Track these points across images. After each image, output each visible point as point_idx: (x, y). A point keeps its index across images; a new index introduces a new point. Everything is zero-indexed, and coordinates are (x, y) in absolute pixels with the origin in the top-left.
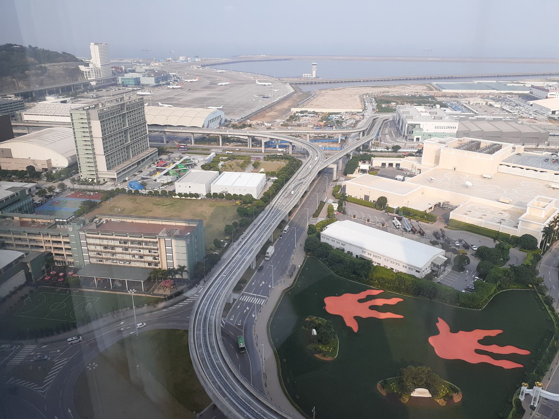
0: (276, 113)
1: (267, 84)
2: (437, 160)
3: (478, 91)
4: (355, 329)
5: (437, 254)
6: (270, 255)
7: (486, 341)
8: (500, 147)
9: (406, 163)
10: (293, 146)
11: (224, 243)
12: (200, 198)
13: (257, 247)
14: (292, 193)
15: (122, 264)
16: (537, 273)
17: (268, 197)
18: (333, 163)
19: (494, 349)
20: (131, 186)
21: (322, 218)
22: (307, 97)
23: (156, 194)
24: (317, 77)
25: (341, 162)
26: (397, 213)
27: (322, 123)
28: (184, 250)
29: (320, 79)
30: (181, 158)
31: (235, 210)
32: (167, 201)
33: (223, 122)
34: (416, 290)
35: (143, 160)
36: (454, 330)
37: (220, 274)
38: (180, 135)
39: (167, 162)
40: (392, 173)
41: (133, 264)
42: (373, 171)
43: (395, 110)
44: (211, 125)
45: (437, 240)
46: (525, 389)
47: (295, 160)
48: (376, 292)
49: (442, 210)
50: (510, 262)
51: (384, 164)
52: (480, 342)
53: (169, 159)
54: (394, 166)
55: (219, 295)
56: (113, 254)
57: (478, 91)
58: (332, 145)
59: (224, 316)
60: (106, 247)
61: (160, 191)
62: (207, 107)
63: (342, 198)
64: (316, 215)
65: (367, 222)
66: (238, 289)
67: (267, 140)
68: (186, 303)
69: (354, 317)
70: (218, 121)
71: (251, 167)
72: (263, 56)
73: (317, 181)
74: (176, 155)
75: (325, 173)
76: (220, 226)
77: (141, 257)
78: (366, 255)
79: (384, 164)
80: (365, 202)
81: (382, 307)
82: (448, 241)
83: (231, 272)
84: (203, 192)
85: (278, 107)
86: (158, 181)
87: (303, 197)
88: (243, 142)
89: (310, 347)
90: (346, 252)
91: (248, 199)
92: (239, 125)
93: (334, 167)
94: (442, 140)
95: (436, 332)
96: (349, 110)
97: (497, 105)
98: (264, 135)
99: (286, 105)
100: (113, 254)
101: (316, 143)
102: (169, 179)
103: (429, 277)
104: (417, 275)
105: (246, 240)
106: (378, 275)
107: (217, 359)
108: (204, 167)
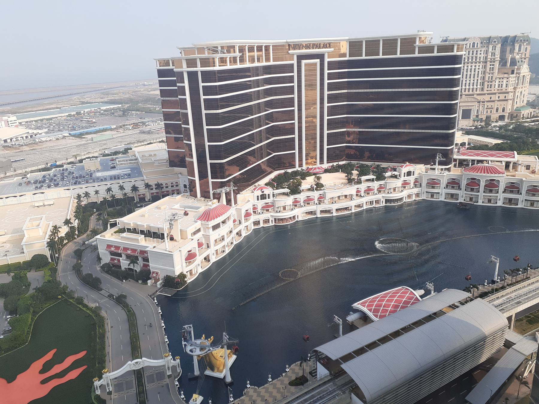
16: (60, 283)
19: (57, 369)
46: (97, 383)
50: (33, 286)
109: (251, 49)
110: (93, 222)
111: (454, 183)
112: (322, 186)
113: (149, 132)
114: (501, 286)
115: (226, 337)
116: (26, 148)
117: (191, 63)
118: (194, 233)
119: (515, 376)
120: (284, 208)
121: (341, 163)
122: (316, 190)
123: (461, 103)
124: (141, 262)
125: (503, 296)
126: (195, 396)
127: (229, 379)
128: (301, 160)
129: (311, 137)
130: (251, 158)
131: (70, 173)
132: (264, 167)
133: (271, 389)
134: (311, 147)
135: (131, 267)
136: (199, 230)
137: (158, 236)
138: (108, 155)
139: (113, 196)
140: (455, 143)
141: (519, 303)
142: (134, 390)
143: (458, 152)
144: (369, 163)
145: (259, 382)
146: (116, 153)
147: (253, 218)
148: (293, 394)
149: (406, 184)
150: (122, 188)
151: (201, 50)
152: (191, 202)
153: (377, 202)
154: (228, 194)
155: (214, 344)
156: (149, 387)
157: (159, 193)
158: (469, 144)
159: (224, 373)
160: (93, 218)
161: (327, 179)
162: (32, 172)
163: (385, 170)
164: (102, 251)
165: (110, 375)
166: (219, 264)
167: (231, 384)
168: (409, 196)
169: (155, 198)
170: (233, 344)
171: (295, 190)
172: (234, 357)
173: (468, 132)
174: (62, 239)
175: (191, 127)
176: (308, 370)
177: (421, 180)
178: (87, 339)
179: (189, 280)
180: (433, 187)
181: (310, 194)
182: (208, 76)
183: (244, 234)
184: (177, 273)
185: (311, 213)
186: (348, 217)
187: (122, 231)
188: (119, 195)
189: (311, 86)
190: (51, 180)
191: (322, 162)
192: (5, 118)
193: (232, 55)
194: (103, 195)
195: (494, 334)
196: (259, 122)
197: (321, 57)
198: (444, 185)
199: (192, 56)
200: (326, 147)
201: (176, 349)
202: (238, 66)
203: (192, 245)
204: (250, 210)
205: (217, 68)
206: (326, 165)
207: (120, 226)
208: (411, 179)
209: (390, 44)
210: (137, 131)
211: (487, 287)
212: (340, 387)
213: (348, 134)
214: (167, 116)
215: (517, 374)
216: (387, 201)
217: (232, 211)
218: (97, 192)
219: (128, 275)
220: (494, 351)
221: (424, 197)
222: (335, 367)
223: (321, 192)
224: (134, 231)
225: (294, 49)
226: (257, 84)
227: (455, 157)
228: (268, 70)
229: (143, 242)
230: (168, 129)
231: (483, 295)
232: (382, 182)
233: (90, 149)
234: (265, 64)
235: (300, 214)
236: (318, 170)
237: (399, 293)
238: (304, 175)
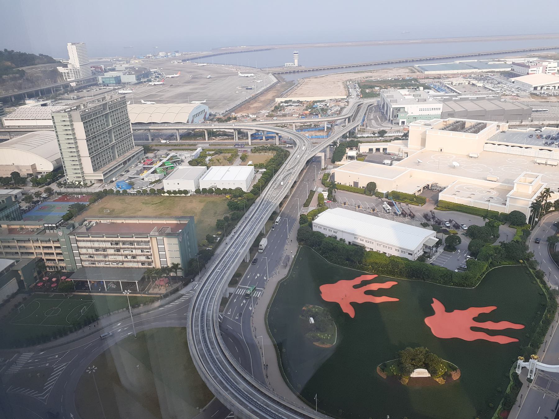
0: (261, 104)
1: (249, 75)
2: (423, 143)
3: (460, 71)
4: (352, 314)
5: (429, 235)
6: (263, 247)
7: (481, 318)
8: (484, 126)
9: (393, 147)
10: (280, 137)
11: (216, 238)
12: (189, 195)
13: (250, 240)
14: (282, 183)
15: (115, 265)
16: (527, 248)
17: (257, 190)
18: (321, 152)
19: (489, 325)
20: (118, 186)
21: (313, 207)
22: (290, 86)
23: (145, 192)
24: (299, 66)
25: (328, 149)
26: (387, 197)
27: (307, 112)
28: (177, 247)
29: (303, 68)
30: (168, 155)
33: (207, 116)
34: (413, 274)
35: (129, 159)
36: (449, 309)
38: (165, 132)
39: (154, 159)
40: (379, 157)
41: (126, 265)
42: (360, 157)
43: (379, 95)
44: (195, 120)
45: (428, 221)
46: (521, 362)
47: (282, 151)
49: (431, 191)
50: (499, 240)
51: (371, 150)
52: (475, 319)
53: (156, 157)
54: (381, 151)
55: (215, 291)
56: (105, 256)
57: (460, 71)
58: (318, 134)
59: (221, 311)
60: (97, 250)
61: (148, 190)
63: (331, 185)
64: (306, 205)
65: (357, 208)
66: (233, 283)
67: (254, 132)
69: (351, 303)
70: (202, 116)
71: (238, 160)
73: (305, 171)
74: (162, 152)
75: (313, 162)
77: (134, 257)
78: (359, 241)
79: (371, 150)
80: (354, 189)
81: (380, 292)
82: (439, 223)
83: (225, 266)
84: (191, 188)
85: (262, 98)
86: (146, 179)
87: (293, 187)
90: (338, 239)
91: (238, 192)
92: (224, 118)
93: (322, 155)
94: (428, 122)
95: (431, 312)
96: (333, 98)
97: (480, 84)
98: (249, 127)
99: (269, 96)
100: (105, 256)
101: (303, 133)
102: (157, 177)
103: (422, 259)
104: (410, 258)
105: (238, 233)
107: (217, 354)
108: (191, 163)
162: (549, 125)
165: (536, 365)
174: (549, 205)
192: (545, 64)
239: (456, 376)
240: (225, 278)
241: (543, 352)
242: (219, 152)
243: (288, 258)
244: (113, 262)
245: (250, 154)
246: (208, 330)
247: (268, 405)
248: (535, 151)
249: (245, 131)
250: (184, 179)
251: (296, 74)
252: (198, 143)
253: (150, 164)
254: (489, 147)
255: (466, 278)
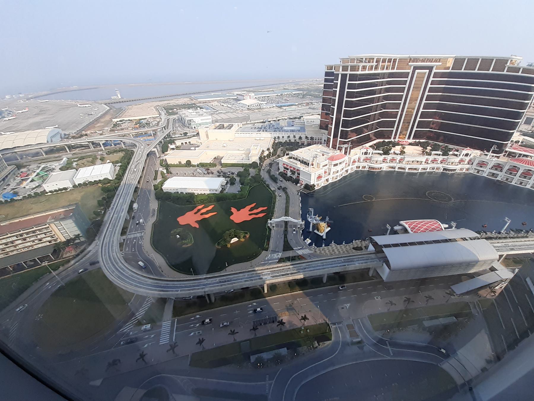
0: (103, 124)
1: (87, 106)
5: (222, 180)
6: (136, 208)
7: (251, 210)
8: (232, 126)
9: (193, 140)
10: (124, 143)
13: (126, 207)
15: (26, 249)
17: (120, 177)
19: (255, 211)
20: (5, 197)
21: (159, 179)
22: (120, 112)
23: (30, 196)
24: (122, 98)
25: (158, 146)
27: (137, 126)
28: (74, 225)
29: (125, 99)
30: (39, 167)
31: (100, 191)
32: (43, 199)
33: (63, 136)
34: (220, 200)
35: (7, 176)
37: (107, 230)
38: (30, 151)
39: (28, 172)
40: (189, 147)
41: (35, 247)
42: (178, 148)
44: (53, 139)
45: (220, 174)
46: (269, 221)
47: (128, 151)
48: (200, 207)
49: (218, 160)
50: (251, 175)
51: (182, 143)
52: (249, 211)
53: (29, 170)
56: (15, 246)
58: (149, 138)
59: (121, 250)
60: (6, 244)
61: (32, 194)
62: (44, 128)
63: (167, 166)
64: (155, 179)
65: (185, 175)
67: (104, 142)
68: (90, 254)
69: (196, 222)
70: (59, 136)
71: (99, 161)
72: (75, 87)
73: (148, 161)
74: (33, 166)
75: (150, 154)
76: (92, 203)
77: (40, 240)
79: (182, 143)
80: (180, 165)
81: (207, 212)
82: (225, 173)
83: (114, 226)
84: (70, 185)
86: (27, 187)
87: (143, 171)
88: (87, 147)
89: (179, 244)
91: (106, 181)
92: (77, 136)
93: (155, 150)
94: (207, 126)
95: (232, 214)
96: (151, 116)
98: (101, 139)
99: (107, 118)
100: (15, 246)
101: (138, 138)
102: (36, 184)
103: (221, 192)
104: (217, 193)
106: (199, 199)
108: (61, 169)
109: (384, 61)
110: (279, 152)
111: (498, 167)
112: (404, 152)
113: (313, 109)
114: (504, 236)
115: (327, 219)
116: (257, 111)
117: (345, 68)
118: (324, 166)
119: (490, 286)
120: (377, 162)
121: (421, 141)
122: (400, 154)
123: (527, 113)
124: (296, 174)
125: (502, 242)
126: (308, 239)
127: (324, 237)
128: (396, 135)
129: (407, 122)
130: (365, 130)
131: (273, 126)
132: (371, 136)
133: (343, 247)
134: (405, 128)
135: (292, 176)
136: (326, 165)
137: (306, 163)
138: (291, 119)
139: (290, 140)
140: (511, 139)
141: (512, 249)
142: (283, 229)
143: (511, 146)
144: (441, 144)
145: (339, 243)
146: (295, 118)
147: (357, 164)
148: (353, 253)
149: (463, 161)
150: (294, 137)
151: (352, 60)
152: (325, 149)
153: (438, 169)
154: (346, 149)
155: (322, 220)
156: (289, 229)
157: (311, 142)
158: (522, 142)
159: (323, 234)
160: (279, 150)
161: (409, 149)
163: (451, 150)
164: (281, 166)
166: (333, 184)
167: (324, 239)
168: (461, 169)
169: (309, 145)
170: (330, 223)
171: (386, 153)
172: (329, 228)
173: (525, 134)
175: (336, 108)
176: (364, 245)
177: (474, 161)
178: (268, 202)
179: (316, 188)
180: (481, 167)
181: (395, 156)
182: (353, 77)
183: (349, 172)
184: (312, 184)
185: (392, 167)
186: (415, 174)
187: (290, 158)
188: (293, 140)
189: (417, 88)
190: (265, 128)
191: (409, 138)
193: (371, 64)
194: (286, 139)
195: (485, 262)
196: (376, 108)
197: (430, 68)
198: (490, 167)
199: (346, 64)
200: (415, 129)
201: (304, 217)
202: (373, 72)
203: (321, 171)
204: (359, 158)
205: (360, 72)
206: (411, 141)
207: (290, 155)
208: (467, 159)
209: (486, 62)
210: (308, 107)
211: (494, 235)
212: (379, 258)
213: (434, 123)
214: (324, 100)
215: (491, 286)
216: (444, 169)
217: (346, 158)
218: (284, 137)
219: (290, 179)
220: (481, 269)
221: (471, 171)
222: (379, 249)
223: (402, 156)
224: (296, 159)
225: (413, 62)
226: (382, 84)
227: (507, 149)
228: (391, 75)
229: (299, 166)
230: (323, 107)
231: (487, 239)
232: (446, 157)
233: (284, 115)
234: (390, 71)
235: (385, 167)
236: (404, 143)
237: (439, 229)
238: (395, 144)
239: (248, 236)
240: (117, 232)
241: (275, 215)
242: (82, 158)
243: (154, 210)
244: (24, 248)
245: (106, 156)
246: (117, 263)
247: (168, 284)
248: (255, 135)
249: (97, 142)
250: (58, 180)
251: (122, 103)
252: (62, 155)
253: (27, 176)
254: (237, 135)
255: (242, 195)
